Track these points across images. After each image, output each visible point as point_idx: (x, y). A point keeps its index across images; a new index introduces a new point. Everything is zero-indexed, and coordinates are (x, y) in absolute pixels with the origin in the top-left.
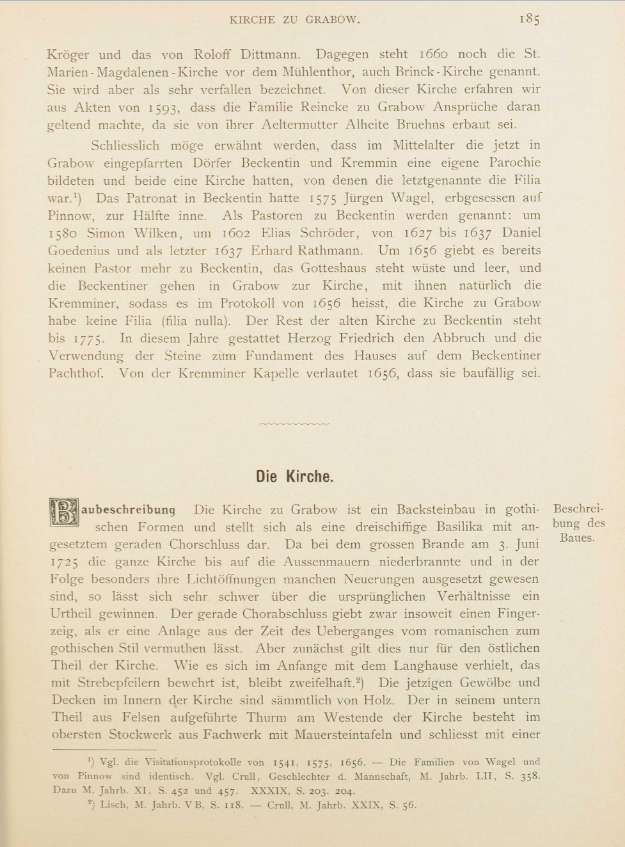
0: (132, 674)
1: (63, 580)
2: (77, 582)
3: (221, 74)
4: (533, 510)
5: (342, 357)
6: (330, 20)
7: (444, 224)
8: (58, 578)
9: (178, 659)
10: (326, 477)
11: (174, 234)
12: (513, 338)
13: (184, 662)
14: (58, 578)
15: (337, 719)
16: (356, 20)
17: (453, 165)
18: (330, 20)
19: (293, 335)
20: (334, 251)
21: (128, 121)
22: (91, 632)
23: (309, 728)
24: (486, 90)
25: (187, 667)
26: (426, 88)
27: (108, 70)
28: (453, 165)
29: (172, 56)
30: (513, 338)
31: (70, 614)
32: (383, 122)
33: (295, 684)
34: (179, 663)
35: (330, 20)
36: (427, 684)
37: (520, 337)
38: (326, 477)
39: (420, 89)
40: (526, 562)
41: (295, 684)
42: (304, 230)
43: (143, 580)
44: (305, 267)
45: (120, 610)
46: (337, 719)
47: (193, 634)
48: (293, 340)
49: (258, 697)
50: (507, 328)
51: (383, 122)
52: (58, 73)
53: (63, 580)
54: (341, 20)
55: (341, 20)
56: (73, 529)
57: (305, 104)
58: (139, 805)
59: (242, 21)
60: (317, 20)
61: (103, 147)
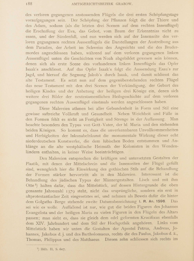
1: (67, 114)
2: (144, 92)
3: (105, 109)
5: (161, 48)
6: (123, 4)
7: (61, 167)
8: (143, 108)
9: (140, 134)
13: (142, 134)
14: (143, 108)
15: (166, 147)
17: (48, 202)
18: (123, 4)
21: (86, 19)
22: (69, 26)
23: (167, 144)
25: (143, 136)
27: (121, 174)
28: (48, 202)
29: (98, 59)
31: (89, 234)
34: (140, 135)
35: (123, 4)
46: (166, 147)
47: (126, 120)
48: (114, 97)
49: (42, 74)
53: (67, 114)
54: (127, 4)
55: (127, 4)
60: (119, 4)
61: (90, 48)
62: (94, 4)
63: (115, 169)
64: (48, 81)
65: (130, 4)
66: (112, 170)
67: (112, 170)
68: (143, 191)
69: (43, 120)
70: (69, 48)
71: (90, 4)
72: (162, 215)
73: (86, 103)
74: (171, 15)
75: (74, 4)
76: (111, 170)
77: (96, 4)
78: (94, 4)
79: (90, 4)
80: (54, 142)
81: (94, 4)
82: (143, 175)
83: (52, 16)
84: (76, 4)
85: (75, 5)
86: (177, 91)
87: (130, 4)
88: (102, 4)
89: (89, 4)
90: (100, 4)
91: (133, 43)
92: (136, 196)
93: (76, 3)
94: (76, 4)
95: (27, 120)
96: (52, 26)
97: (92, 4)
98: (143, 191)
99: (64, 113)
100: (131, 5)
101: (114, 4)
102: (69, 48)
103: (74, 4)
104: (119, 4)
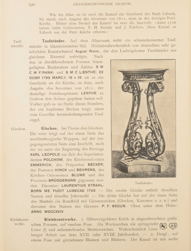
0: (124, 232)
4: (176, 219)
10: (24, 129)
11: (132, 201)
12: (146, 196)
16: (130, 4)
19: (93, 45)
20: (66, 52)
24: (48, 104)
26: (65, 83)
30: (146, 196)
32: (66, 143)
33: (117, 191)
36: (51, 144)
37: (148, 195)
38: (24, 129)
39: (63, 83)
40: (100, 175)
41: (117, 191)
42: (60, 143)
43: (101, 104)
44: (31, 99)
45: (38, 179)
50: (144, 193)
51: (66, 143)
52: (42, 202)
54: (126, 4)
55: (126, 4)
56: (110, 175)
57: (63, 148)
58: (133, 219)
59: (108, 4)
60: (119, 4)
62: (95, 4)
63: (173, 219)
64: (85, 62)
65: (129, 4)
66: (171, 219)
67: (171, 219)
68: (43, 181)
69: (55, 94)
70: (50, 235)
71: (91, 4)
72: (84, 136)
73: (36, 121)
74: (80, 115)
75: (75, 4)
76: (169, 219)
77: (96, 4)
78: (95, 4)
79: (91, 4)
80: (34, 63)
81: (95, 4)
82: (93, 19)
83: (68, 100)
84: (77, 4)
85: (77, 6)
86: (103, 144)
87: (129, 4)
88: (102, 4)
89: (90, 4)
90: (100, 4)
91: (82, 115)
92: (68, 110)
93: (77, 4)
94: (77, 4)
95: (81, 41)
96: (75, 165)
97: (92, 4)
98: (43, 181)
99: (31, 103)
100: (130, 4)
101: (114, 4)
102: (50, 235)
103: (75, 4)
104: (119, 4)
